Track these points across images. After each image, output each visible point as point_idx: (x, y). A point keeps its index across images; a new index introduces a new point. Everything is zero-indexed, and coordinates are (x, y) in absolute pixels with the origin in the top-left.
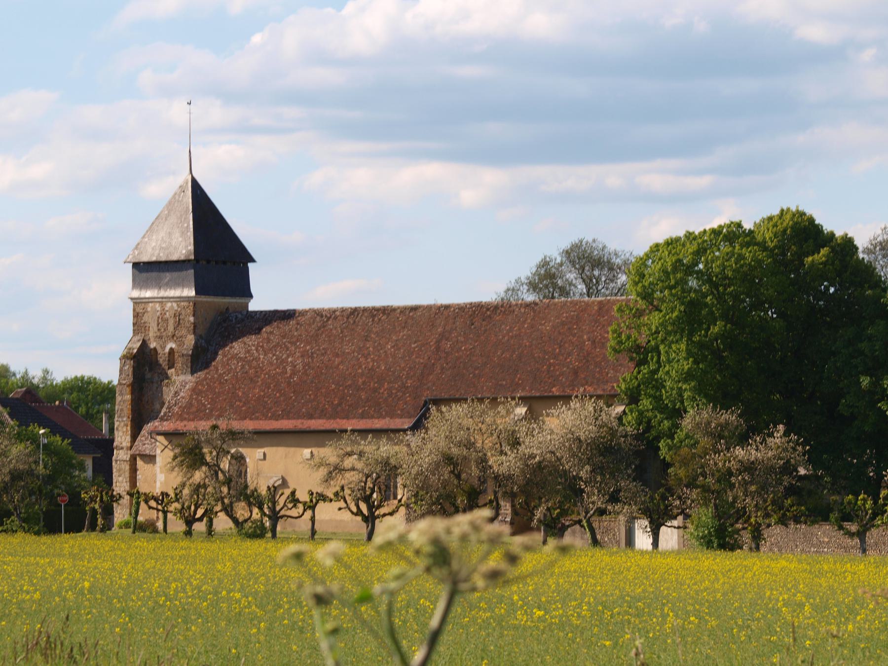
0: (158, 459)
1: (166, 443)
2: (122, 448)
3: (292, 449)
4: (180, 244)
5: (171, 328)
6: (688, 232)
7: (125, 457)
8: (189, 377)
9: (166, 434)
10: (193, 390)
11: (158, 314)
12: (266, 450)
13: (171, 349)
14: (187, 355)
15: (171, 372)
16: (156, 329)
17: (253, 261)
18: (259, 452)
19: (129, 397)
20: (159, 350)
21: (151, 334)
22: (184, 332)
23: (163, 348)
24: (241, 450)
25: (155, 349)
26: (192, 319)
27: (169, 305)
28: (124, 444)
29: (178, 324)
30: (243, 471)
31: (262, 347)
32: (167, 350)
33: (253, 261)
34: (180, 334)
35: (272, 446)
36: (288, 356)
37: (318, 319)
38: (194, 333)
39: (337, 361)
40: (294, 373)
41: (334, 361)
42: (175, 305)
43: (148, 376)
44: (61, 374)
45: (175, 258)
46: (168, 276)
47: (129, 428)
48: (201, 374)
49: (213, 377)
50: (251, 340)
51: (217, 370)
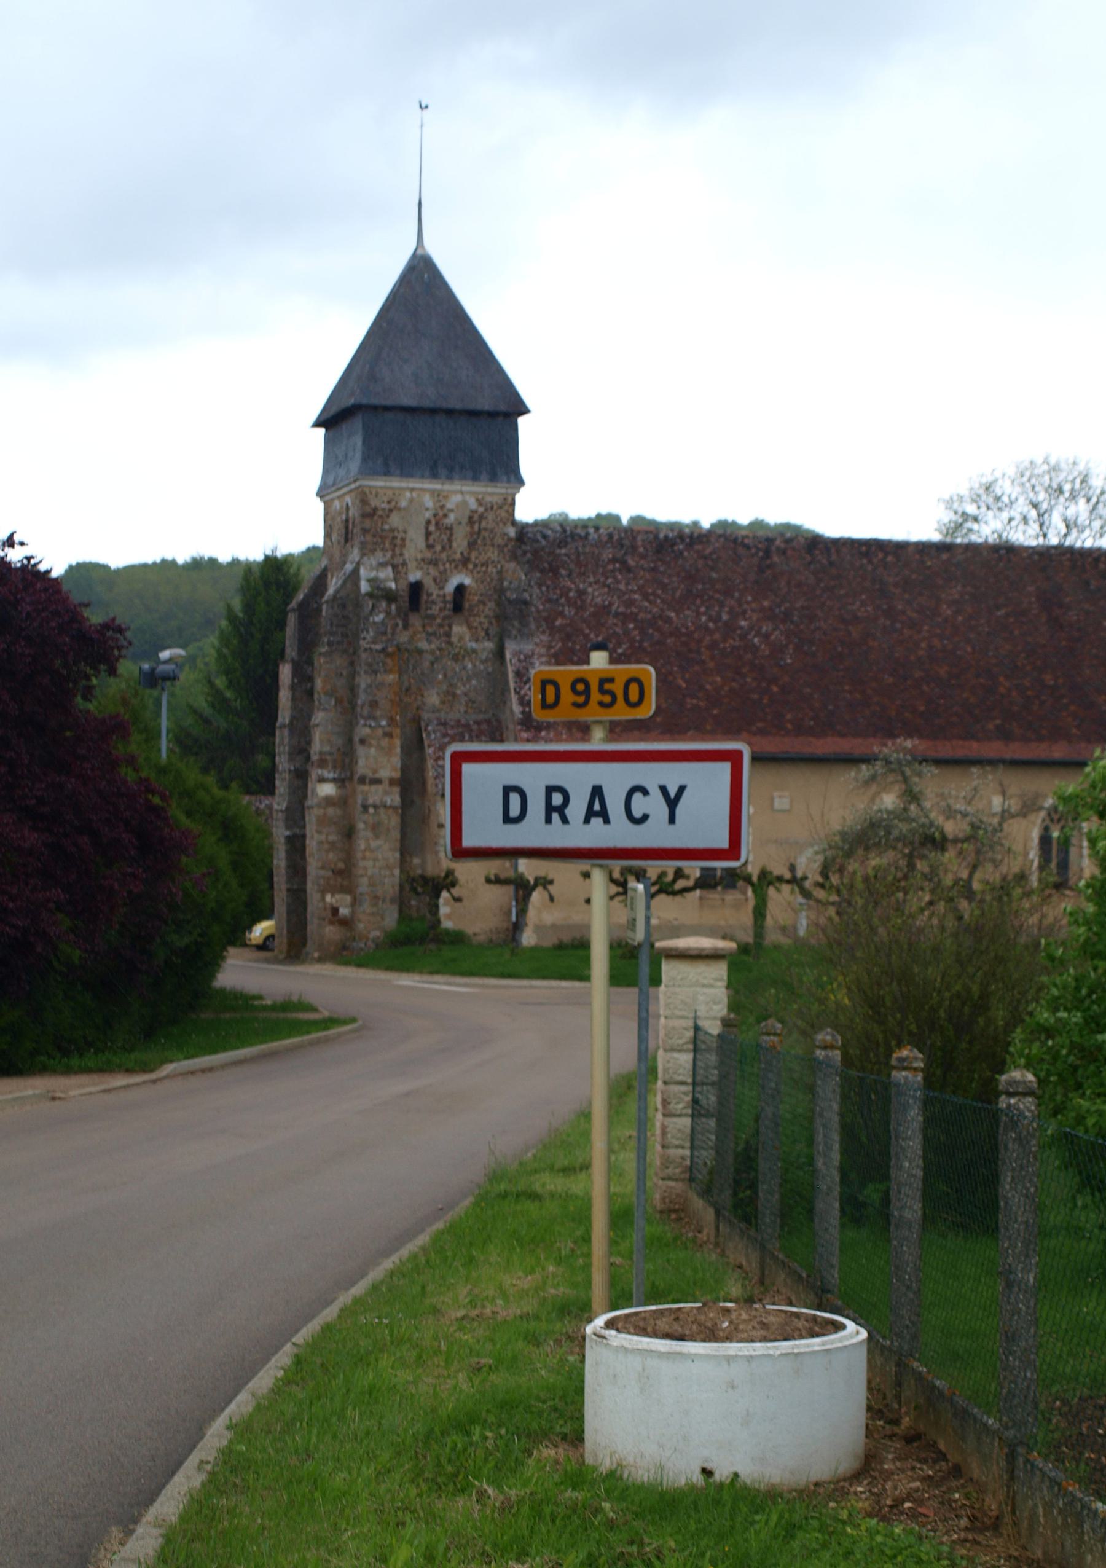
5: (460, 543)
11: (428, 515)
13: (460, 589)
16: (421, 544)
23: (440, 582)
32: (450, 587)
34: (483, 558)
47: (398, 742)
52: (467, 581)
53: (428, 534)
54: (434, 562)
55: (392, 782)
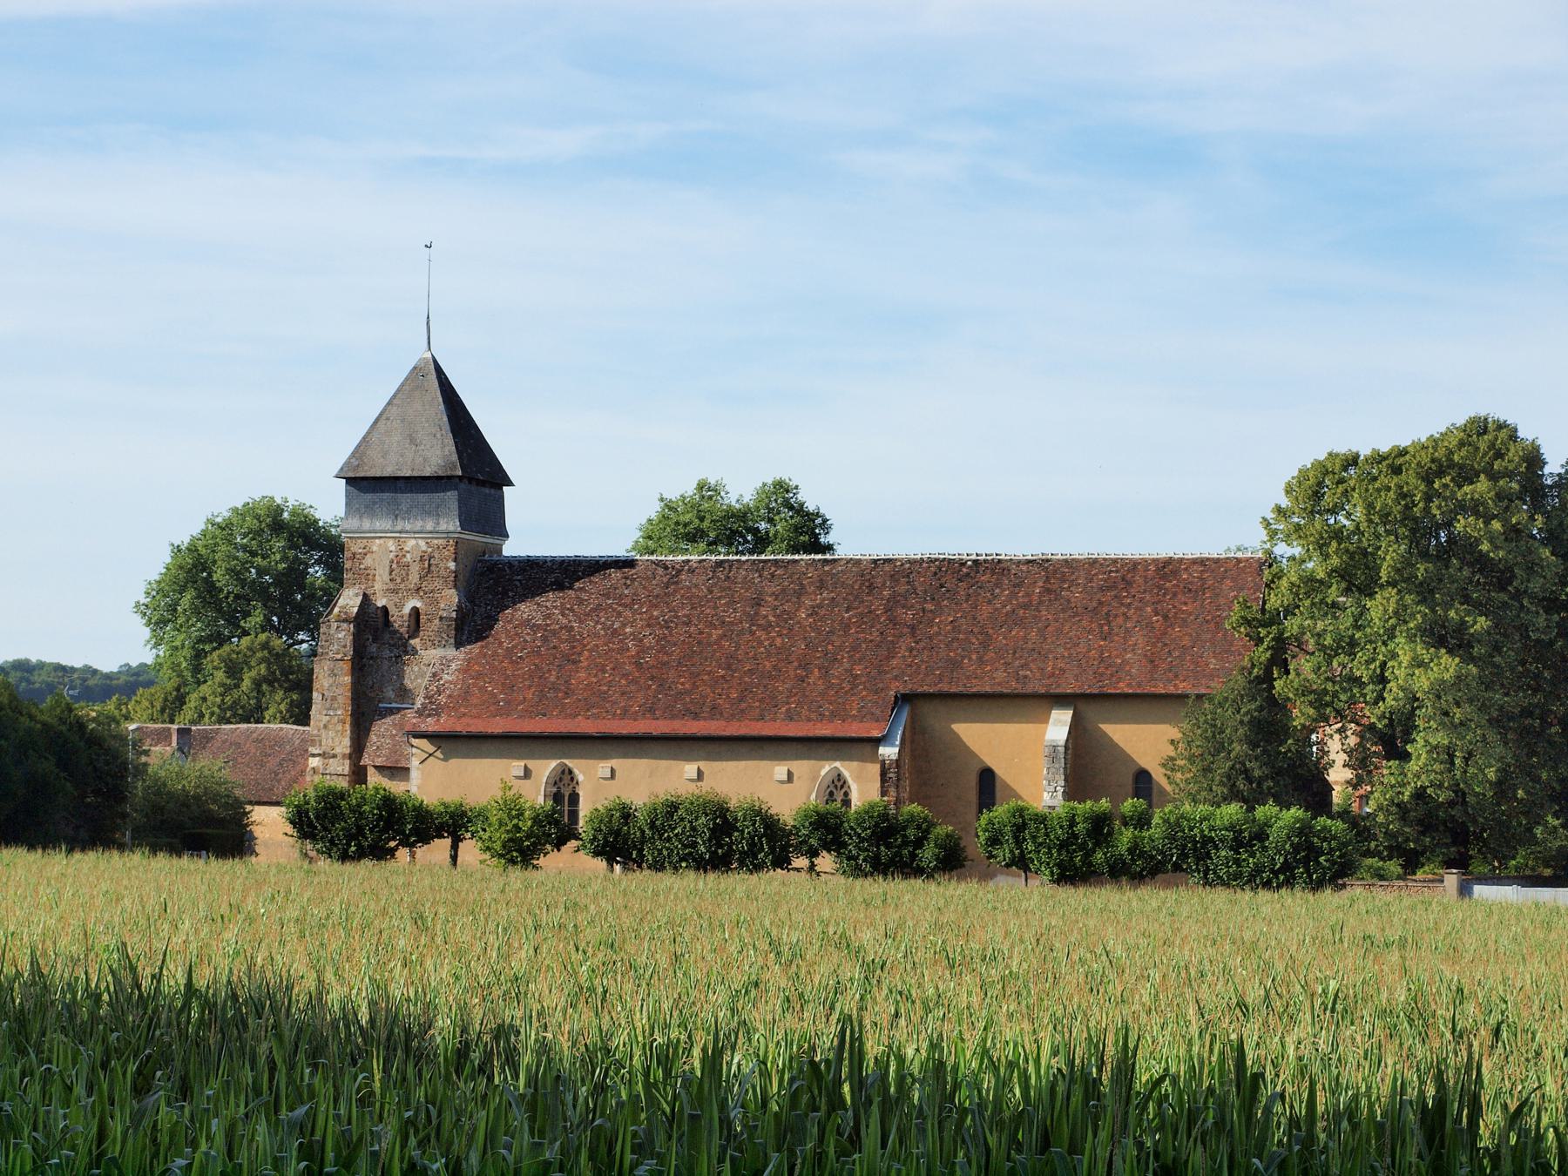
0: (414, 774)
1: (431, 749)
2: (334, 756)
3: (664, 763)
4: (435, 453)
5: (414, 578)
6: (1330, 454)
7: (340, 770)
8: (451, 652)
9: (431, 737)
10: (464, 671)
11: (392, 556)
12: (614, 763)
13: (416, 612)
14: (451, 619)
15: (415, 642)
16: (386, 578)
17: (510, 484)
18: (603, 767)
19: (348, 679)
20: (392, 610)
21: (378, 586)
22: (438, 584)
23: (400, 606)
24: (569, 763)
25: (385, 609)
26: (452, 565)
27: (412, 542)
28: (338, 750)
29: (427, 572)
30: (908, 744)
31: (571, 610)
32: (407, 610)
33: (510, 484)
34: (430, 587)
35: (625, 756)
36: (624, 625)
37: (660, 571)
38: (455, 586)
39: (716, 633)
40: (642, 651)
41: (710, 635)
42: (422, 543)
43: (373, 648)
44: (77, 663)
45: (386, 474)
46: (405, 499)
47: (348, 727)
48: (475, 648)
49: (495, 654)
50: (551, 599)
51: (501, 643)
52: (419, 605)
53: (391, 571)
54: (396, 591)
55: (344, 756)
